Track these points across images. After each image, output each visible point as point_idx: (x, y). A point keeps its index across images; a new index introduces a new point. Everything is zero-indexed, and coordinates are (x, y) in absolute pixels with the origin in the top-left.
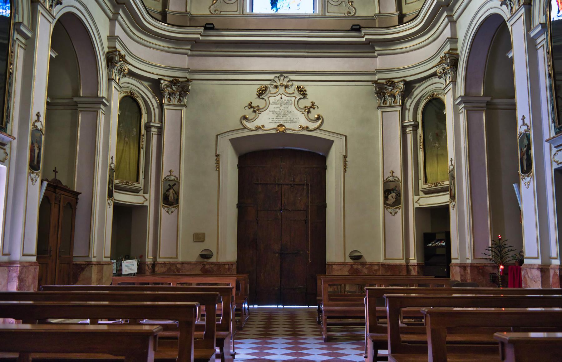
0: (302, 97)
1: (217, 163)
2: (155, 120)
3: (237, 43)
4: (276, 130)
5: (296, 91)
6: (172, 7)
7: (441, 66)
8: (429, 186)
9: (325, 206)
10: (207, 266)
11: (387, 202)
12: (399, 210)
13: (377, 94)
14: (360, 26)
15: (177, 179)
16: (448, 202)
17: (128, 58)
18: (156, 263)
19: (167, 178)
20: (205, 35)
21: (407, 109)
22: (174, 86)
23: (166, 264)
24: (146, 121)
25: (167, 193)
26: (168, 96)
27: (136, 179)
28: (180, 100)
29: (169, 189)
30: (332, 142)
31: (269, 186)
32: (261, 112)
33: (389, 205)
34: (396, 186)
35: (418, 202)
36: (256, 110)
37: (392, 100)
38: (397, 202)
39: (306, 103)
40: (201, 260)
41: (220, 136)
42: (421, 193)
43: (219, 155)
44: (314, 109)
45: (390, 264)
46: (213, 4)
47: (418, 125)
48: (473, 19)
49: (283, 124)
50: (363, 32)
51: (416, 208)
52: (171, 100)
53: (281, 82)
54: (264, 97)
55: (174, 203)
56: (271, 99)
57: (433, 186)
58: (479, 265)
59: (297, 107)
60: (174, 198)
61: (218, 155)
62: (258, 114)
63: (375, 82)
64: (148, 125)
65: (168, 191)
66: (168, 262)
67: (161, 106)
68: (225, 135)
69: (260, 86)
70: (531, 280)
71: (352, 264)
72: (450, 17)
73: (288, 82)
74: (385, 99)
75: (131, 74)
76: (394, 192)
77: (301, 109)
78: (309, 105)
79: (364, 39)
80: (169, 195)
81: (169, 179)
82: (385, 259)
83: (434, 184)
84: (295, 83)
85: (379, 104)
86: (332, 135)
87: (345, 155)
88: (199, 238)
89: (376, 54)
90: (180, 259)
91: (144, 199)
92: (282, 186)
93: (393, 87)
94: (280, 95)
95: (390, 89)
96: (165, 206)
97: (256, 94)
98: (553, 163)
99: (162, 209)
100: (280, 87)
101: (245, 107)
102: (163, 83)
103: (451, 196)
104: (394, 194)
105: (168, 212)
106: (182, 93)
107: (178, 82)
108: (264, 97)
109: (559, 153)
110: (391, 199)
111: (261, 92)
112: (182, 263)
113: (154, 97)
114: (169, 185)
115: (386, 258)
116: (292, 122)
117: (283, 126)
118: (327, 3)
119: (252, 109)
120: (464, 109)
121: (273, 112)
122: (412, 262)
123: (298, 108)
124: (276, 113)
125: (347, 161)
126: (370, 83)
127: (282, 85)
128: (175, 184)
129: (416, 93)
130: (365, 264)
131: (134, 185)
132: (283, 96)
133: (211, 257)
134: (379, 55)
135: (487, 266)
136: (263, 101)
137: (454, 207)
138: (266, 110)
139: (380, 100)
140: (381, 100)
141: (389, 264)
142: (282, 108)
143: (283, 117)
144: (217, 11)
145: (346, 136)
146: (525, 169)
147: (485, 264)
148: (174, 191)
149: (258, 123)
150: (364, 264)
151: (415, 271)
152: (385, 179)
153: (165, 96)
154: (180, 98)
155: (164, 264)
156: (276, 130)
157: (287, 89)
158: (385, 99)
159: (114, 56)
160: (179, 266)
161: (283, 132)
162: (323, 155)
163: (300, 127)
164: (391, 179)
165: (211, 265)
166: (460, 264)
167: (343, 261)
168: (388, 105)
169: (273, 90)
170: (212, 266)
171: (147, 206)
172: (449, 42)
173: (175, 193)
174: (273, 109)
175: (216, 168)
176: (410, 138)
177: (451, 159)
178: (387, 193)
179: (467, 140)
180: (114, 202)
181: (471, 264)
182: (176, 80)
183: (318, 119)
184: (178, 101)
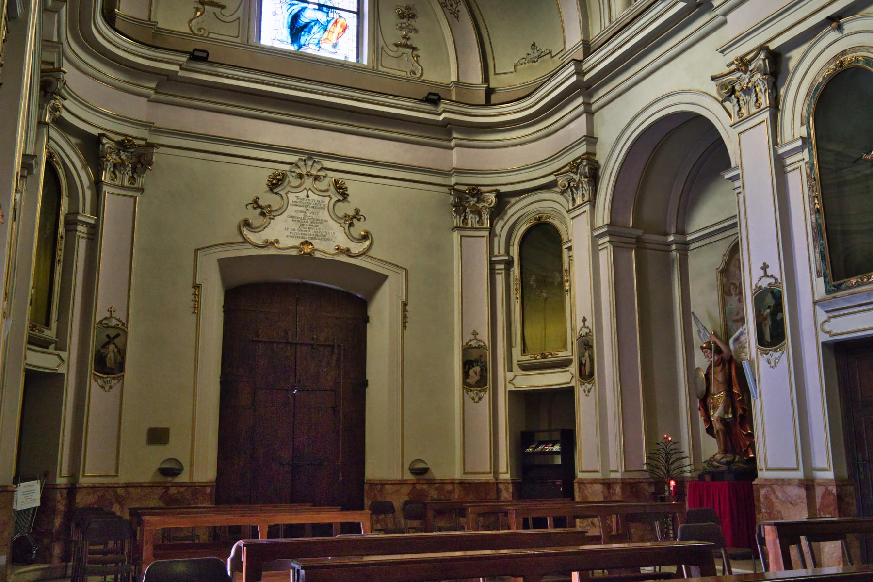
0: (341, 198)
1: (196, 301)
2: (84, 211)
3: (235, 91)
4: (298, 250)
5: (332, 188)
6: (123, 9)
7: (566, 176)
8: (530, 357)
9: (365, 384)
10: (173, 491)
11: (468, 381)
12: (485, 394)
13: (454, 206)
14: (440, 96)
15: (123, 324)
18: (78, 486)
19: (103, 322)
20: (189, 68)
21: (496, 235)
22: (123, 151)
23: (96, 488)
24: (67, 212)
25: (102, 351)
26: (112, 169)
27: (44, 321)
28: (132, 179)
29: (108, 343)
30: (386, 277)
31: (275, 346)
32: (274, 216)
33: (470, 385)
34: (481, 356)
35: (513, 381)
36: (266, 213)
37: (476, 218)
38: (482, 382)
39: (347, 209)
40: (160, 479)
41: (202, 251)
42: (516, 368)
43: (199, 287)
44: (359, 220)
45: (472, 482)
46: (196, 17)
47: (513, 261)
48: (639, 114)
49: (310, 240)
50: (442, 107)
51: (510, 392)
52: (116, 177)
53: (308, 170)
54: (280, 190)
55: (115, 372)
56: (292, 197)
57: (538, 357)
58: (632, 481)
59: (332, 214)
60: (115, 361)
61: (197, 287)
62: (269, 220)
63: (451, 187)
64: (71, 218)
65: (105, 346)
66: (100, 485)
67: (97, 185)
68: (210, 252)
69: (274, 171)
70: (783, 503)
71: (415, 482)
72: (587, 104)
73: (319, 170)
74: (465, 216)
76: (478, 365)
77: (339, 218)
78: (351, 213)
79: (441, 118)
80: (107, 355)
81: (107, 324)
82: (465, 473)
83: (541, 354)
84: (330, 173)
85: (457, 224)
86: (386, 267)
87: (405, 300)
88: (158, 436)
89: (453, 143)
90: (122, 479)
91: (58, 361)
92: (298, 347)
93: (478, 198)
94: (305, 190)
95: (473, 201)
96: (98, 376)
97: (267, 184)
98: (820, 333)
99: (93, 381)
100: (306, 177)
101: (247, 205)
102: (106, 143)
103: (583, 374)
104: (478, 369)
105: (102, 387)
106: (139, 166)
107: (132, 145)
108: (280, 190)
109: (832, 320)
110: (474, 378)
111: (274, 181)
112: (127, 486)
113: (84, 167)
114: (108, 336)
115: (466, 471)
116: (324, 238)
117: (311, 244)
118: (381, 52)
119: (259, 210)
120: (610, 244)
121: (295, 219)
122: (502, 477)
123: (332, 214)
124: (299, 221)
125: (408, 312)
126: (446, 189)
127: (309, 175)
128: (118, 335)
129: (510, 212)
130: (434, 482)
131: (43, 332)
132: (310, 193)
133: (180, 474)
134: (457, 146)
135: (641, 482)
136: (278, 197)
138: (282, 214)
139: (458, 217)
140: (460, 217)
141: (470, 481)
142: (308, 214)
143: (309, 229)
144: (202, 30)
145: (406, 270)
146: (768, 337)
147: (639, 479)
148: (116, 347)
149: (269, 234)
150: (431, 482)
151: (507, 492)
152: (464, 344)
153: (106, 168)
154: (133, 175)
155: (94, 488)
156: (298, 250)
157: (317, 182)
158: (465, 216)
159: (52, 79)
160: (121, 491)
161: (310, 254)
162: (363, 297)
163: (336, 248)
164: (474, 343)
165: (179, 488)
166: (603, 479)
167: (399, 477)
168: (470, 226)
169: (296, 182)
170: (182, 490)
171: (63, 375)
173: (119, 351)
174: (294, 214)
175: (192, 310)
176: (500, 279)
178: (467, 366)
179: (614, 291)
181: (622, 479)
182: (129, 141)
183: (365, 237)
184: (129, 181)
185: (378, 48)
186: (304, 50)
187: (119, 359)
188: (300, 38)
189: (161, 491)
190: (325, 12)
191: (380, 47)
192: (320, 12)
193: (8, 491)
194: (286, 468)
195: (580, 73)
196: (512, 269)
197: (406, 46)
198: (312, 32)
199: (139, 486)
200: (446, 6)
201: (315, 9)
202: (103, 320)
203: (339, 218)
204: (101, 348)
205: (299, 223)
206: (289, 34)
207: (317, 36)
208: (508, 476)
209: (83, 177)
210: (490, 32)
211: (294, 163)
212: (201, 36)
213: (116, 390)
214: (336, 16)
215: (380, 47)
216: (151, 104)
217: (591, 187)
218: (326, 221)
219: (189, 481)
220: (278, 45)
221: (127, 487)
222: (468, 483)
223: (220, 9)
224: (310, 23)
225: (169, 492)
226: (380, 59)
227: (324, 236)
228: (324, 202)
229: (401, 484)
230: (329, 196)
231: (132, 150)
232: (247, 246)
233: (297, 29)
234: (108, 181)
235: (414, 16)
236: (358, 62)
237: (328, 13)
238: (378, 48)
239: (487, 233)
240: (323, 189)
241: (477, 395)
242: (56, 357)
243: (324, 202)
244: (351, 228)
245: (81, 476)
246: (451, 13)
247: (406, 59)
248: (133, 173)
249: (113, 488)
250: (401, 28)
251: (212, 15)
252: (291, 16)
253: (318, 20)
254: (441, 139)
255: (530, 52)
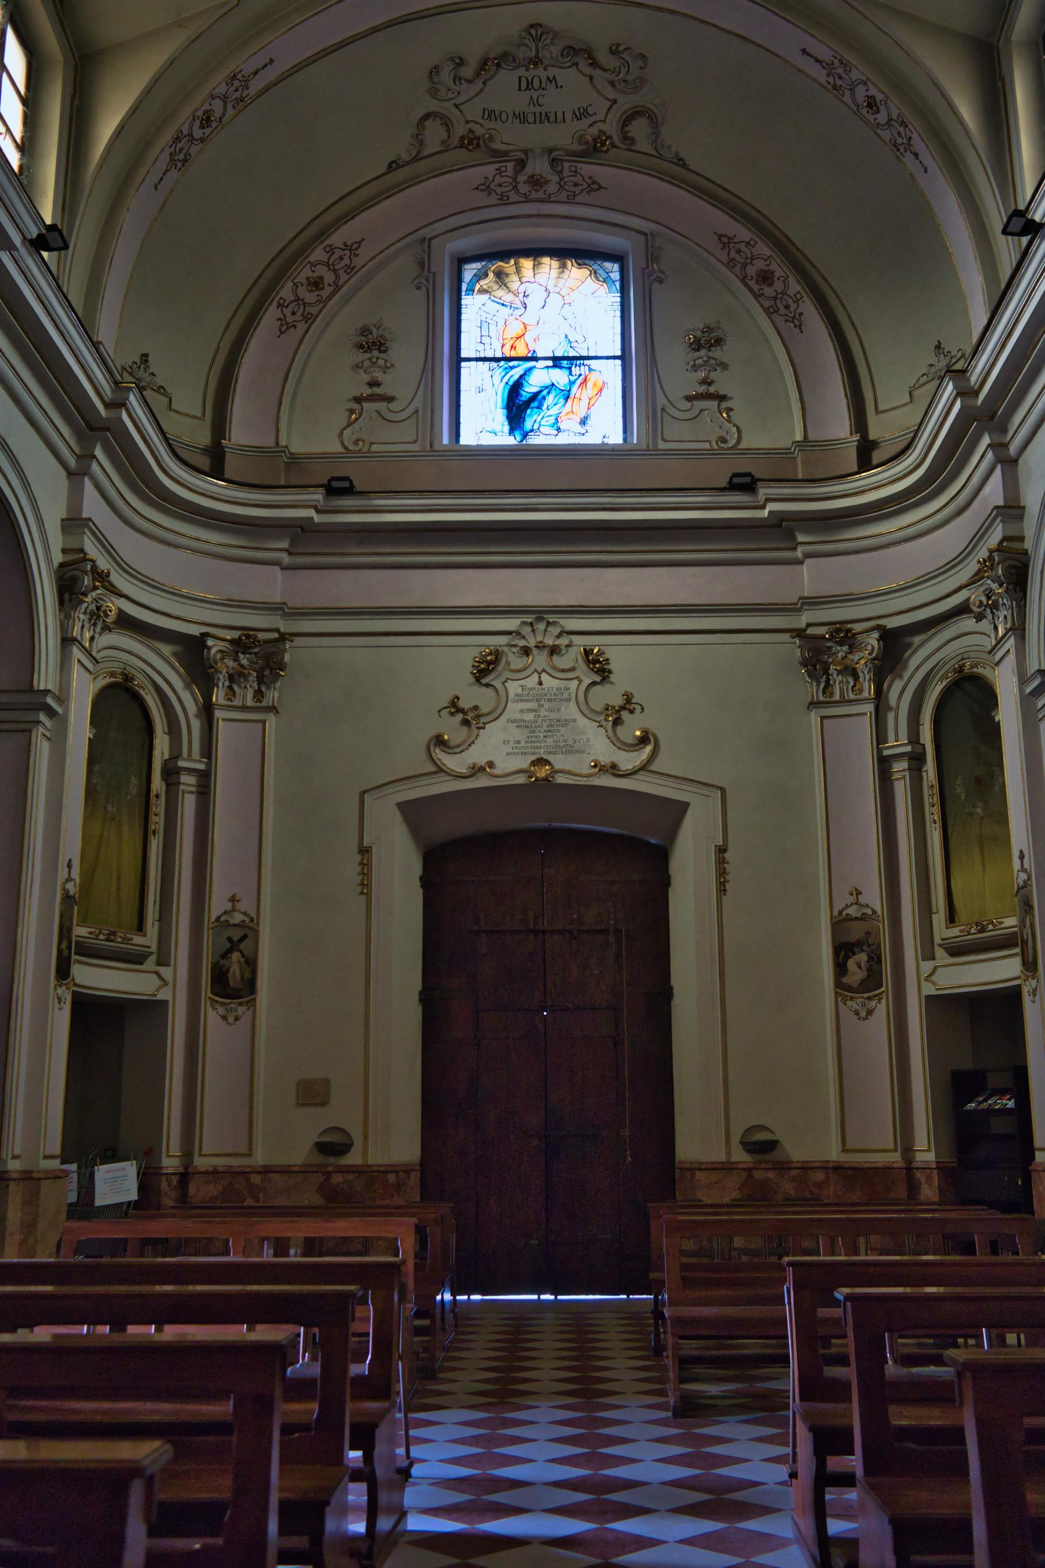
0: (598, 679)
1: (364, 874)
4: (527, 775)
5: (582, 665)
7: (981, 585)
10: (337, 1179)
11: (845, 980)
13: (805, 666)
14: (753, 477)
15: (252, 920)
16: (1018, 978)
17: (117, 579)
19: (222, 919)
21: (890, 709)
22: (242, 653)
23: (219, 1173)
24: (166, 756)
25: (223, 962)
26: (227, 684)
27: (135, 924)
28: (259, 694)
29: (230, 951)
33: (850, 989)
37: (848, 683)
38: (872, 982)
39: (610, 695)
40: (319, 1159)
42: (940, 952)
43: (368, 851)
44: (632, 712)
46: (349, 425)
49: (545, 757)
50: (763, 492)
51: (928, 997)
52: (234, 695)
54: (493, 679)
56: (513, 688)
60: (242, 976)
61: (365, 851)
62: (475, 732)
65: (225, 955)
67: (207, 710)
69: (483, 649)
71: (751, 1165)
73: (559, 636)
74: (828, 681)
75: (126, 623)
76: (862, 951)
78: (618, 701)
79: (765, 513)
80: (229, 969)
81: (227, 921)
83: (977, 924)
84: (577, 639)
87: (721, 843)
89: (799, 553)
90: (260, 1159)
91: (158, 982)
93: (850, 646)
96: (217, 1002)
99: (210, 1009)
100: (535, 651)
101: (439, 711)
104: (863, 957)
105: (224, 1018)
106: (267, 672)
107: (253, 643)
108: (493, 679)
110: (856, 973)
112: (266, 1171)
113: (187, 686)
114: (229, 939)
115: (848, 1147)
117: (547, 762)
119: (460, 717)
121: (519, 724)
124: (527, 727)
126: (786, 637)
127: (540, 646)
128: (245, 937)
129: (913, 663)
131: (132, 939)
132: (544, 676)
134: (808, 555)
136: (490, 691)
137: (1035, 995)
139: (814, 684)
141: (856, 1165)
142: (543, 713)
144: (360, 443)
145: (723, 790)
148: (243, 956)
149: (476, 755)
150: (783, 1166)
151: (931, 1185)
152: (836, 913)
155: (214, 1173)
157: (555, 658)
158: (828, 681)
159: (78, 573)
160: (256, 1179)
161: (546, 779)
163: (593, 764)
164: (853, 911)
167: (723, 1158)
168: (837, 697)
170: (351, 1177)
171: (165, 1003)
172: (999, 518)
173: (247, 961)
175: (359, 889)
177: (1021, 852)
178: (843, 953)
180: (74, 992)
182: (248, 637)
183: (644, 740)
184: (254, 698)
185: (654, 411)
186: (534, 440)
187: (247, 974)
188: (524, 420)
189: (317, 1179)
190: (564, 367)
191: (659, 408)
192: (557, 370)
193: (31, 1179)
194: (536, 1142)
195: (965, 392)
196: (925, 769)
197: (708, 396)
198: (544, 407)
199: (285, 1171)
200: (777, 311)
201: (548, 367)
202: (221, 916)
203: (596, 712)
204: (220, 959)
205: (527, 730)
206: (505, 418)
207: (554, 411)
208: (931, 1157)
209: (187, 701)
210: (863, 338)
211: (514, 632)
212: (359, 451)
213: (245, 1020)
214: (584, 370)
215: (659, 408)
216: (285, 572)
217: (1014, 603)
218: (575, 721)
219: (362, 1163)
220: (488, 440)
221: (267, 1172)
222: (850, 1168)
223: (386, 404)
224: (541, 391)
225: (391, 1182)
226: (659, 428)
227: (571, 746)
228: (567, 689)
229: (724, 1169)
230: (577, 678)
231: (256, 650)
232: (443, 777)
233: (519, 406)
234: (222, 701)
235: (719, 342)
236: (625, 439)
237: (570, 369)
238: (654, 411)
239: (870, 708)
240: (566, 667)
241: (864, 1005)
242: (154, 976)
243: (567, 689)
244: (619, 727)
245: (196, 1154)
246: (786, 321)
247: (708, 420)
248: (259, 684)
249: (243, 1174)
250: (695, 368)
251: (374, 415)
252: (508, 387)
253: (553, 385)
254: (777, 549)
255: (933, 360)
